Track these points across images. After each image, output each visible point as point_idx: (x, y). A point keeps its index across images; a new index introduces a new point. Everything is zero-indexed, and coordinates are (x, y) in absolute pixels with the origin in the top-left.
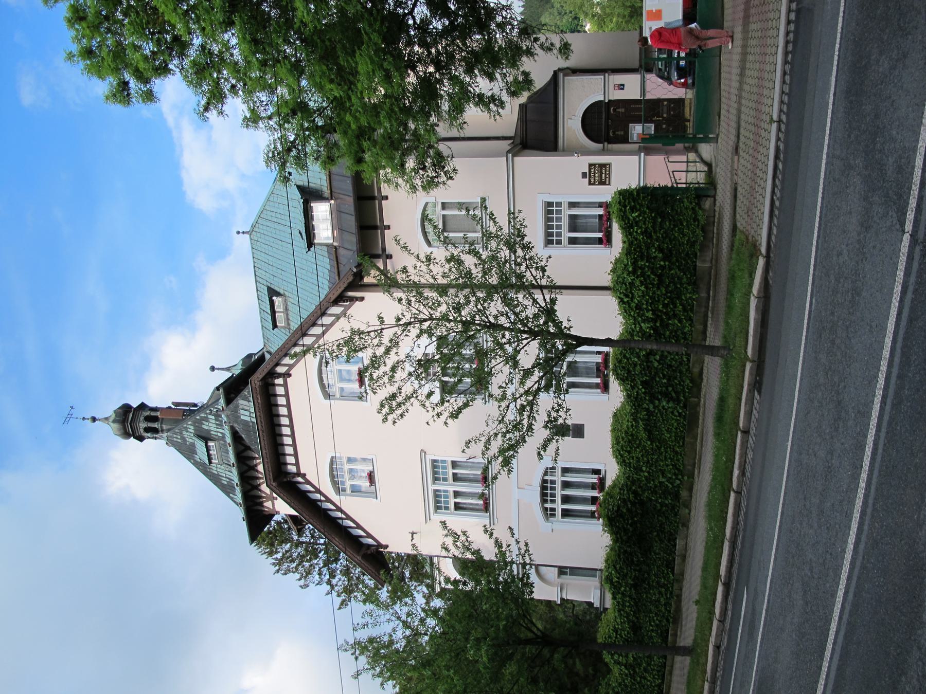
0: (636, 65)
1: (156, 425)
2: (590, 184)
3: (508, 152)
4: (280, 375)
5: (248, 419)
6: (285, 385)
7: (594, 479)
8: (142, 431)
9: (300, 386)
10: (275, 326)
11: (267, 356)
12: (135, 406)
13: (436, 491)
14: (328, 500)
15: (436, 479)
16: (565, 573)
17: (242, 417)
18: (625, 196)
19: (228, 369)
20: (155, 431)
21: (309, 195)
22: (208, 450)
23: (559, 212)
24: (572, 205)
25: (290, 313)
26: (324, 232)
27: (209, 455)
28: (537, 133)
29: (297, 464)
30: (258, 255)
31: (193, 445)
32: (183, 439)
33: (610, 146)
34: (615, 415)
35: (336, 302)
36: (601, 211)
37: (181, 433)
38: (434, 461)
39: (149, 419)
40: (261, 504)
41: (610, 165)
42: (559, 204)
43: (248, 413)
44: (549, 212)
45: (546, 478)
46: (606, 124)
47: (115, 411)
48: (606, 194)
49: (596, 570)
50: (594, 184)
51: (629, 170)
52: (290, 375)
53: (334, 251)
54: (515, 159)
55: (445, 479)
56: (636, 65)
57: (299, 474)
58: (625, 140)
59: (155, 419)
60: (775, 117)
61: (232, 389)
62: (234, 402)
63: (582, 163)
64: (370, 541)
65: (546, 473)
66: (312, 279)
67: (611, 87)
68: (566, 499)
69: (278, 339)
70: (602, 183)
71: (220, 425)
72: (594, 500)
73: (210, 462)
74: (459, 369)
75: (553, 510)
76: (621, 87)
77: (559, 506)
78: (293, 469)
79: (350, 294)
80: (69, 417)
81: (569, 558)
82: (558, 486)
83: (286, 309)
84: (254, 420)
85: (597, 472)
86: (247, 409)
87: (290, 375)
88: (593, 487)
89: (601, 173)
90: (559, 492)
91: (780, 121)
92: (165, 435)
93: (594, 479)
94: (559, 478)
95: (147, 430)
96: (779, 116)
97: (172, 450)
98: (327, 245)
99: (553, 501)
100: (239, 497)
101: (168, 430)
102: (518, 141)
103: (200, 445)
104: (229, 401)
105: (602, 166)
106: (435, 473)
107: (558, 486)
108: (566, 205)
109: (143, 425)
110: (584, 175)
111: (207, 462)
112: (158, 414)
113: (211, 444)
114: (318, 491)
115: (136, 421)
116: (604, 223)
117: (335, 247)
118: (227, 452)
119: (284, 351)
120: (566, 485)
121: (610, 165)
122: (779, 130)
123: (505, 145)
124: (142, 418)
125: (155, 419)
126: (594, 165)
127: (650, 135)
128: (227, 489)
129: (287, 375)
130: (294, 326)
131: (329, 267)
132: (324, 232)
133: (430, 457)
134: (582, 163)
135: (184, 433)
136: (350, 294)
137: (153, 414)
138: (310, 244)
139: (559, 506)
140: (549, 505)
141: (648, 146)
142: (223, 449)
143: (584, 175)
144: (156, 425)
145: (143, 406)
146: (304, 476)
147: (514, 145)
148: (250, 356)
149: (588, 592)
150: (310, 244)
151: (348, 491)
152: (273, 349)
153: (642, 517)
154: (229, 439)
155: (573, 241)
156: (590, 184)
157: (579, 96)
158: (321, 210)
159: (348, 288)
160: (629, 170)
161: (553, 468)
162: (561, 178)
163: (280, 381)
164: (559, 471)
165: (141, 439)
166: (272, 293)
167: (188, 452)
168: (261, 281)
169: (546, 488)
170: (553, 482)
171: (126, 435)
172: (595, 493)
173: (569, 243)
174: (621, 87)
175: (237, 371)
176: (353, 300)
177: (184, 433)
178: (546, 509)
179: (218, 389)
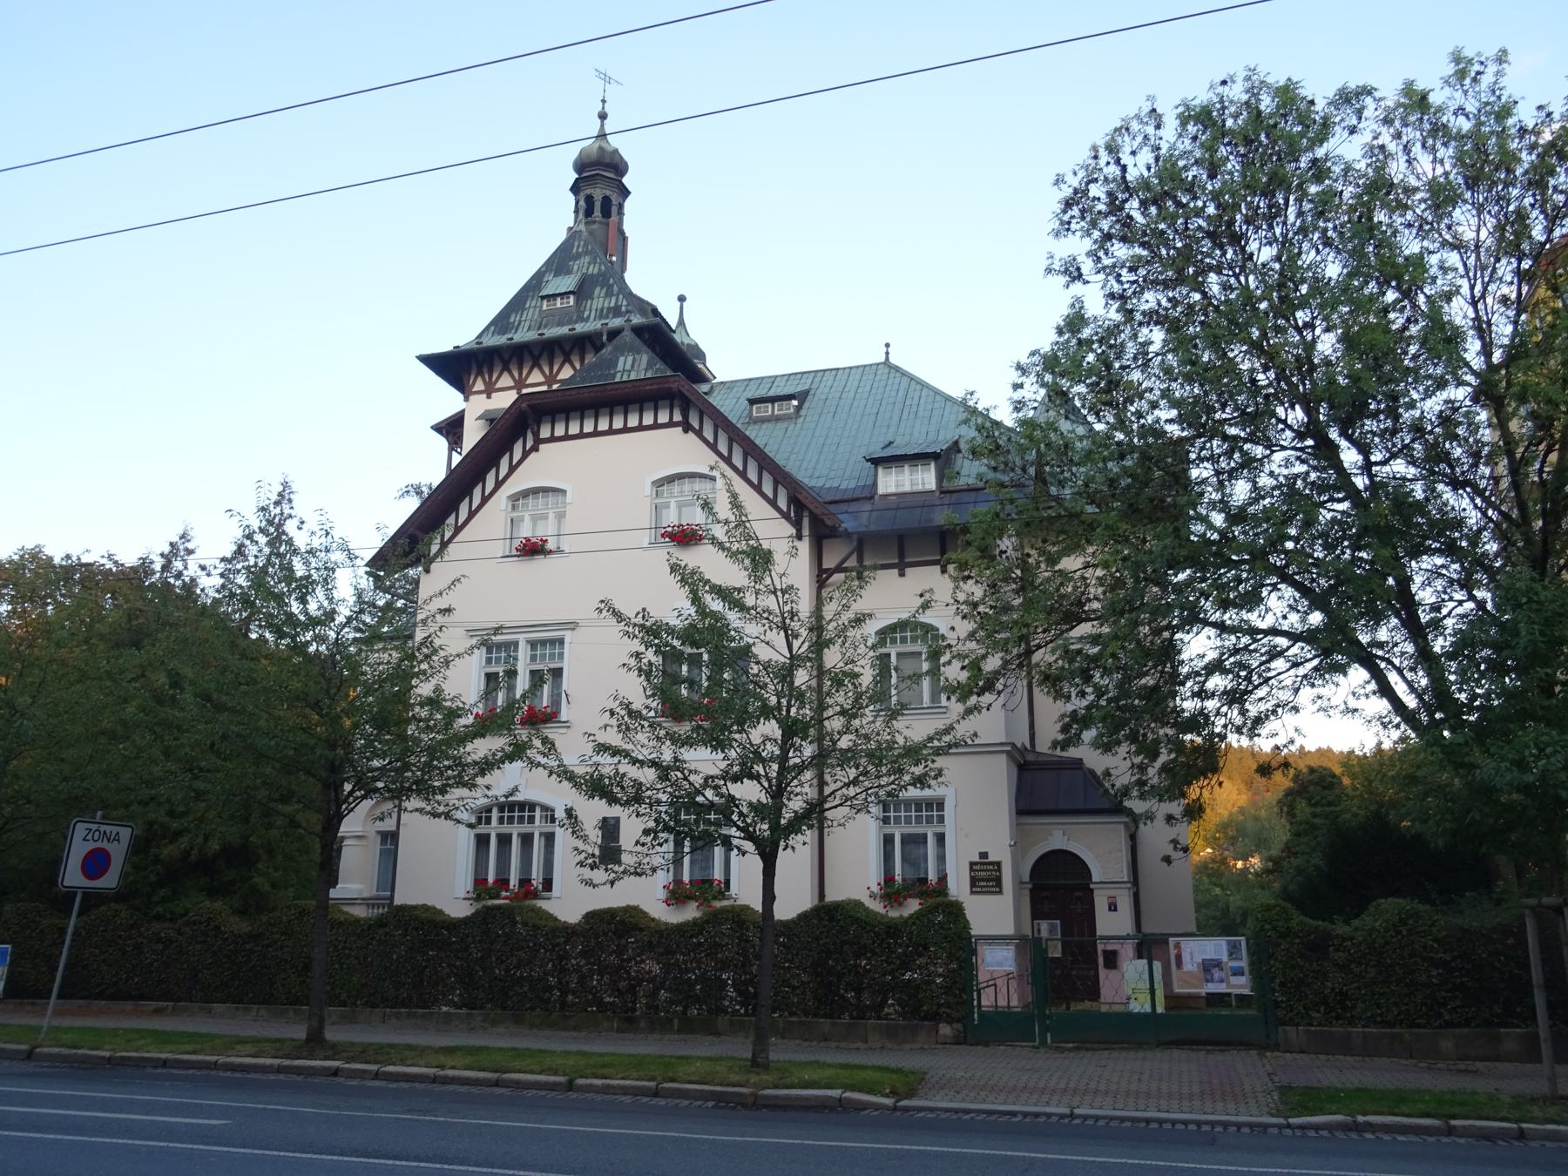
0: (1147, 928)
1: (597, 213)
2: (972, 864)
3: (1013, 745)
4: (685, 416)
5: (620, 366)
6: (671, 424)
7: (536, 875)
8: (588, 192)
9: (669, 448)
10: (752, 402)
11: (704, 388)
12: (625, 180)
13: (516, 644)
14: (499, 484)
15: (533, 644)
16: (384, 842)
17: (622, 359)
18: (955, 911)
19: (681, 322)
20: (589, 212)
21: (942, 459)
22: (562, 295)
23: (929, 820)
24: (941, 839)
25: (770, 425)
26: (891, 482)
27: (554, 296)
28: (1042, 786)
29: (553, 439)
30: (856, 375)
31: (569, 272)
32: (578, 256)
33: (1027, 892)
34: (636, 908)
35: (793, 500)
36: (932, 876)
37: (586, 253)
38: (561, 642)
39: (606, 201)
40: (480, 373)
41: (1000, 892)
42: (941, 819)
43: (628, 367)
44: (929, 806)
45: (538, 810)
46: (1058, 887)
47: (616, 151)
48: (958, 886)
49: (393, 890)
50: (971, 870)
51: (993, 917)
52: (686, 431)
53: (869, 494)
54: (1004, 757)
55: (533, 658)
56: (1147, 928)
57: (538, 441)
58: (1037, 915)
59: (606, 213)
60: (1077, 1111)
61: (657, 336)
62: (645, 348)
63: (1001, 851)
64: (435, 548)
65: (545, 808)
66: (821, 457)
67: (1112, 893)
68: (505, 840)
69: (730, 406)
70: (974, 882)
71: (601, 314)
72: (503, 882)
73: (543, 298)
74: (697, 676)
75: (488, 821)
76: (1113, 907)
77: (494, 829)
78: (545, 432)
79: (806, 522)
80: (607, 79)
81: (433, 862)
82: (526, 828)
83: (778, 419)
84: (617, 379)
85: (548, 884)
86: (633, 366)
87: (686, 431)
88: (525, 882)
89: (988, 880)
90: (515, 830)
91: (1072, 1116)
92: (582, 227)
93: (536, 875)
94: (538, 827)
95: (590, 200)
96: (1079, 1116)
97: (563, 236)
98: (875, 484)
99: (501, 820)
100: (490, 341)
101: (591, 233)
102: (1030, 757)
103: (567, 283)
104: (638, 330)
105: (998, 881)
106: (543, 642)
107: (526, 828)
108: (939, 830)
109: (598, 194)
110: (984, 855)
111: (544, 293)
112: (614, 218)
113: (572, 300)
114: (512, 469)
115: (600, 181)
116: (919, 886)
117: (872, 498)
118: (560, 324)
119: (721, 422)
120: (527, 840)
121: (1000, 892)
122: (1062, 1116)
123: (1022, 739)
124: (608, 193)
125: (606, 213)
126: (999, 870)
127: (1046, 951)
128: (501, 322)
129: (687, 428)
130: (751, 432)
131: (843, 487)
132: (891, 482)
133: (568, 636)
134: (1001, 851)
135: (587, 259)
136: (806, 522)
137: (614, 209)
138: (876, 462)
139: (494, 829)
140: (495, 814)
141: (1028, 946)
142: (563, 318)
143: (984, 855)
144: (597, 213)
145: (625, 193)
146: (535, 449)
147: (1023, 751)
148: (701, 356)
149: (354, 882)
150: (876, 462)
151: (514, 514)
152: (714, 400)
153: (503, 961)
154: (580, 328)
155: (888, 840)
156: (972, 864)
157: (1099, 849)
158: (925, 479)
159: (813, 515)
160: (993, 917)
161: (553, 820)
162: (976, 818)
163: (677, 417)
164: (548, 828)
165: (575, 189)
166: (803, 396)
167: (559, 262)
168: (817, 380)
169: (522, 809)
170: (531, 820)
171: (581, 166)
172: (514, 881)
173: (885, 836)
174: (1113, 907)
175: (677, 337)
176: (797, 525)
177: (587, 259)
178: (489, 810)
179: (655, 312)
